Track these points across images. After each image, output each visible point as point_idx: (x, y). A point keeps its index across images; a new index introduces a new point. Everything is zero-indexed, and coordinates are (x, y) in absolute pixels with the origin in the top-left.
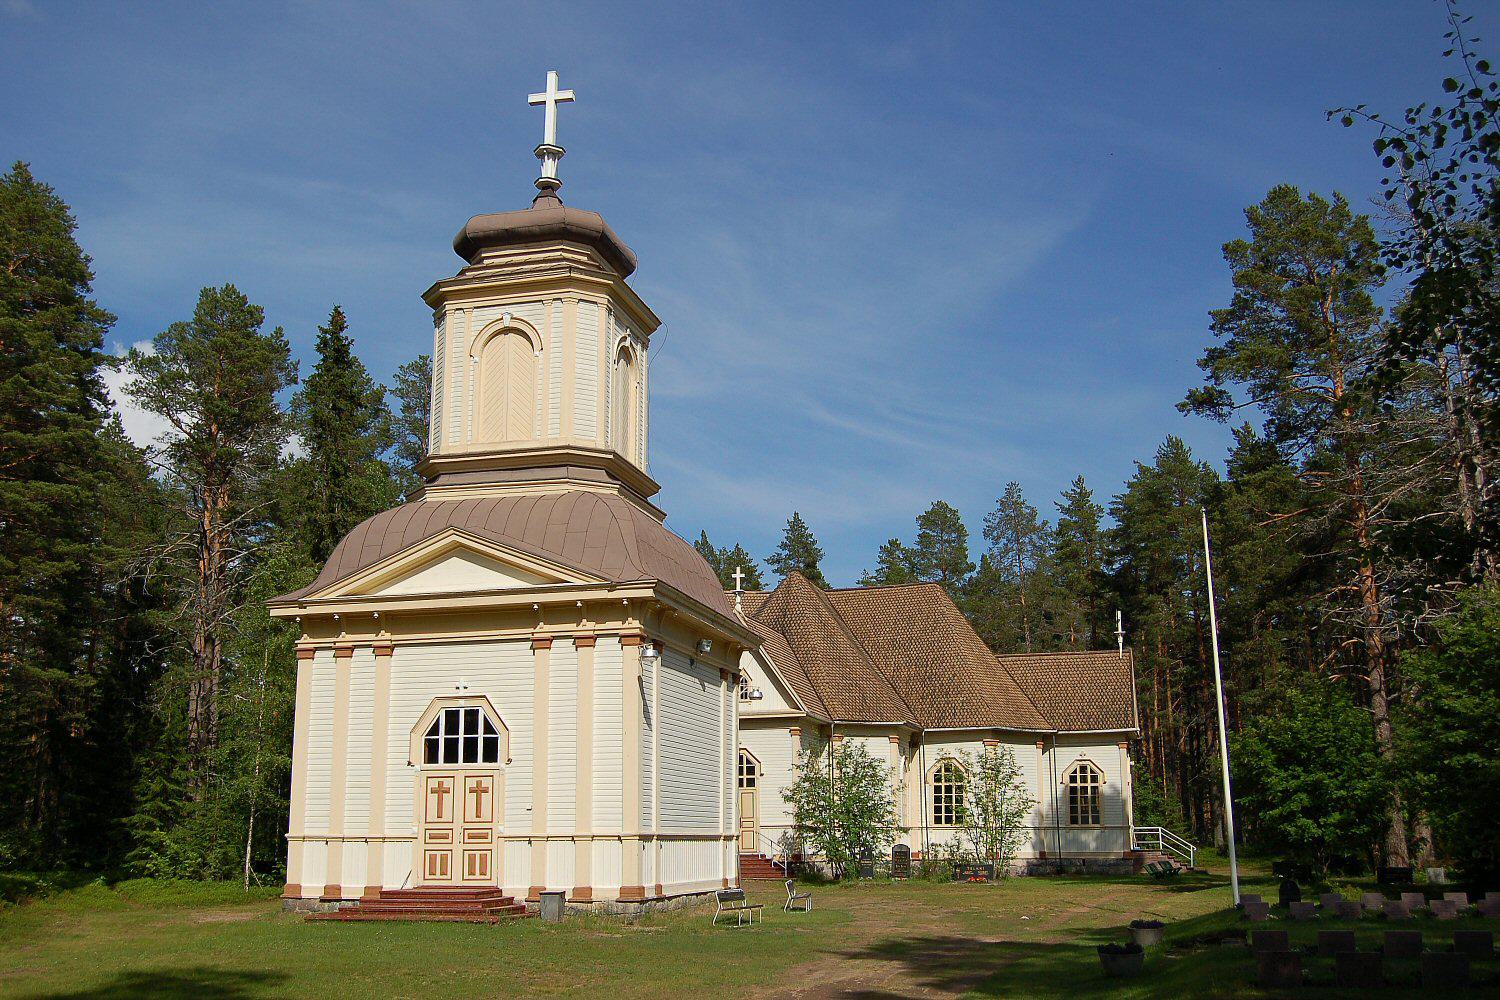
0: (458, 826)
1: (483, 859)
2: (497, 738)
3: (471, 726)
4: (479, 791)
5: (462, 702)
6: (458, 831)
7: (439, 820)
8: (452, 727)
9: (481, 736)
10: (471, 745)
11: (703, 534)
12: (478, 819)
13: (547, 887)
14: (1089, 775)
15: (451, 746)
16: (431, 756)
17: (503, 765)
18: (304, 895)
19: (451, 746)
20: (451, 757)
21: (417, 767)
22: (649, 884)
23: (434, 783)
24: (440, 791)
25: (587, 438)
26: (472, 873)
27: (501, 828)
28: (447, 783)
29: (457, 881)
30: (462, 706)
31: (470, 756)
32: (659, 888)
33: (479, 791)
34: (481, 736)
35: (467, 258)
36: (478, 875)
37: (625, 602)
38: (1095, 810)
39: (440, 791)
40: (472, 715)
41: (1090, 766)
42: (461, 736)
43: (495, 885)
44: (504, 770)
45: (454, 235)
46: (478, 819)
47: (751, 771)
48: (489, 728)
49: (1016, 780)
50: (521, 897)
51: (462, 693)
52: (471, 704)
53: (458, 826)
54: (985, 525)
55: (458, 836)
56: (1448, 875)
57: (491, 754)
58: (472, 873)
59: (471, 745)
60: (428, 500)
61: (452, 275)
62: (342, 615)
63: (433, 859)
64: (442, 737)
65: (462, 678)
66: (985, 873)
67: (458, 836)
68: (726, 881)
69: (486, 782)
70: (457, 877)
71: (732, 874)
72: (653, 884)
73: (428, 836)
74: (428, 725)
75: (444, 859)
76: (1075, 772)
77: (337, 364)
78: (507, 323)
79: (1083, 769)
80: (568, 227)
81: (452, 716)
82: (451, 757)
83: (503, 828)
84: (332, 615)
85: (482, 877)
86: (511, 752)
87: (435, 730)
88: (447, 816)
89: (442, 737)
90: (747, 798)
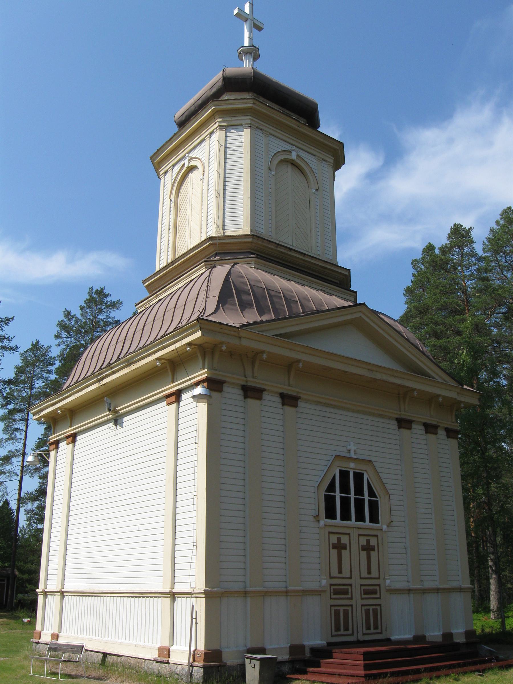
0: (356, 582)
5: (352, 465)
8: (345, 489)
9: (366, 497)
12: (369, 576)
13: (268, 647)
16: (330, 514)
17: (385, 527)
20: (346, 516)
23: (334, 539)
24: (339, 547)
25: (288, 115)
26: (368, 628)
28: (345, 540)
30: (352, 467)
33: (368, 548)
36: (342, 632)
38: (374, 506)
40: (359, 477)
48: (372, 493)
49: (11, 342)
52: (361, 468)
53: (356, 582)
54: (475, 248)
55: (357, 592)
56: (27, 587)
58: (368, 628)
64: (338, 494)
67: (357, 592)
69: (373, 542)
72: (462, 630)
77: (475, 325)
85: (346, 633)
87: (331, 487)
88: (346, 572)
89: (338, 494)
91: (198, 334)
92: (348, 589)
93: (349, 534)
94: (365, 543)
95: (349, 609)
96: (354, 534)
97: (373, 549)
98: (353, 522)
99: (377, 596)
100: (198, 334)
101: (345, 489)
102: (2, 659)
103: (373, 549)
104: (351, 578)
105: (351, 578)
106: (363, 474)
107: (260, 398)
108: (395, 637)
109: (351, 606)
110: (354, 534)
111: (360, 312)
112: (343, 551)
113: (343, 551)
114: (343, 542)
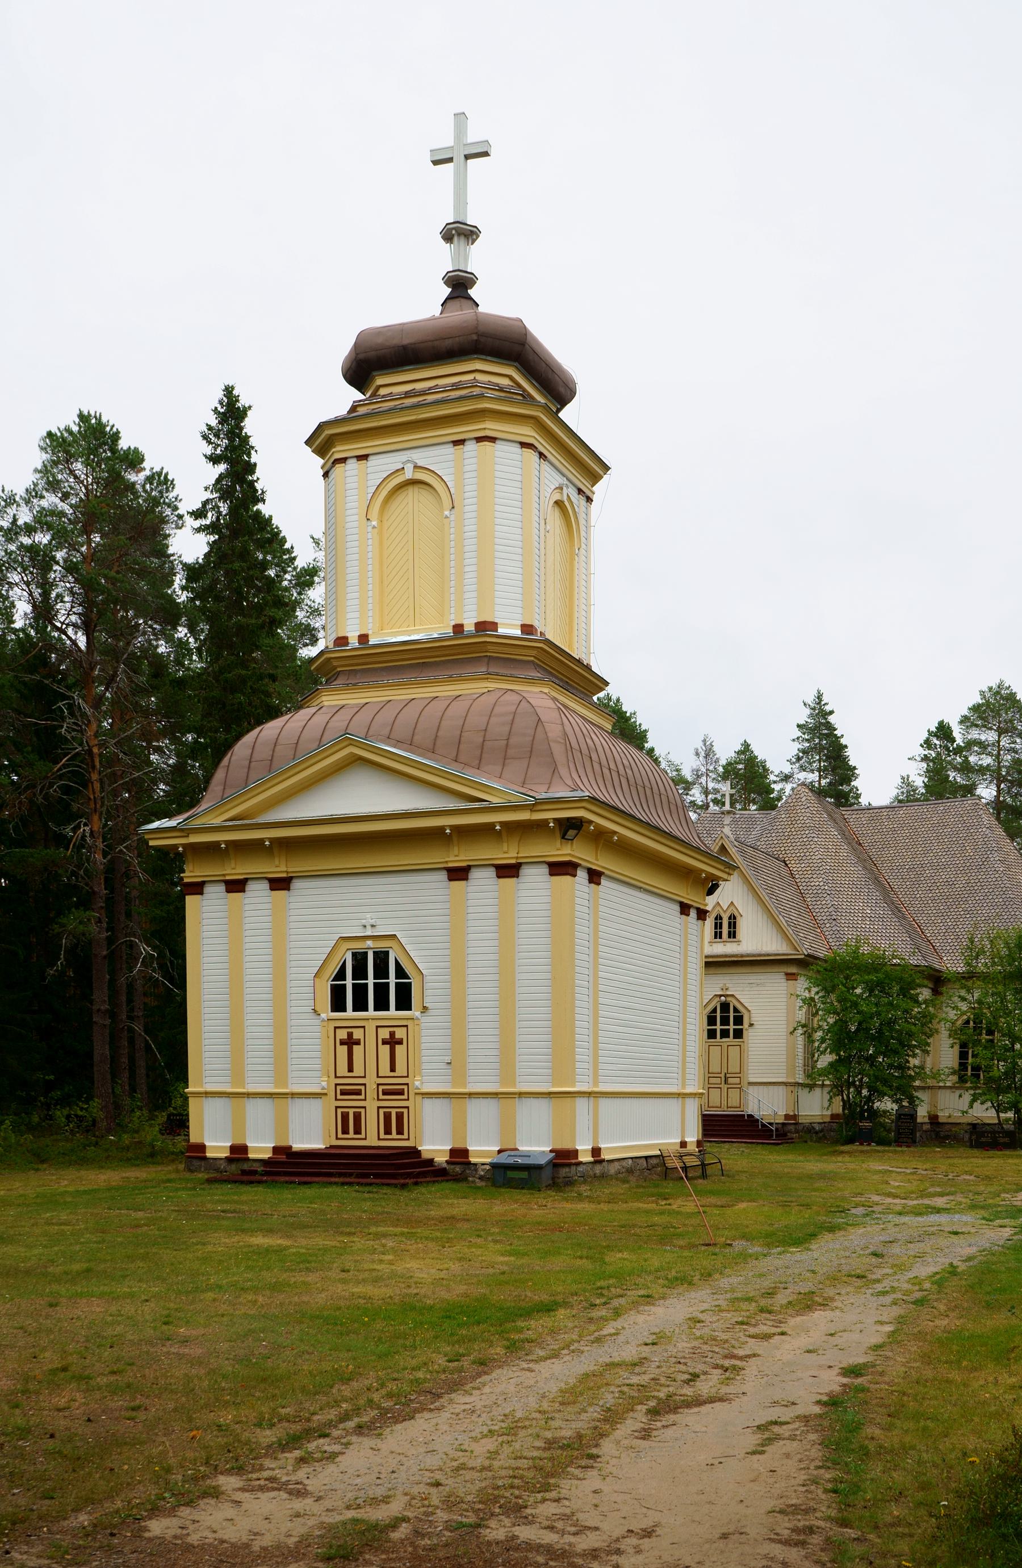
0: (371, 1081)
1: (400, 1117)
2: (410, 983)
3: (381, 970)
4: (393, 1042)
5: (370, 943)
6: (371, 1088)
7: (350, 1074)
8: (360, 971)
9: (392, 980)
10: (381, 991)
11: (842, 735)
12: (392, 1074)
14: (732, 1014)
15: (360, 992)
16: (338, 1004)
17: (417, 1014)
18: (209, 1154)
19: (360, 992)
20: (360, 1005)
21: (323, 1016)
22: (584, 1148)
23: (342, 1034)
24: (350, 1042)
26: (388, 1131)
27: (417, 1083)
28: (357, 1034)
29: (372, 1140)
31: (382, 1004)
32: (596, 1151)
33: (393, 1042)
34: (392, 980)
35: (360, 386)
36: (394, 1135)
37: (498, 827)
39: (350, 1042)
40: (382, 958)
41: (733, 1002)
42: (371, 981)
43: (413, 1145)
44: (418, 1019)
45: (343, 348)
46: (392, 1074)
47: (739, 1020)
48: (400, 972)
50: (441, 1159)
51: (369, 933)
52: (381, 945)
53: (371, 1081)
57: (404, 1002)
58: (388, 1131)
59: (381, 991)
60: (326, 703)
61: (343, 410)
62: (228, 843)
63: (345, 1117)
64: (349, 982)
65: (368, 916)
66: (1006, 1140)
68: (683, 1144)
69: (400, 1033)
70: (372, 1136)
71: (693, 1136)
73: (338, 1092)
74: (333, 969)
75: (357, 1117)
76: (714, 1010)
78: (409, 474)
79: (725, 1007)
80: (482, 339)
81: (360, 960)
82: (360, 1005)
83: (421, 1083)
84: (262, 840)
86: (426, 999)
87: (341, 975)
88: (358, 1070)
89: (349, 982)
90: (734, 1052)
91: (312, 668)
92: (361, 1090)
93: (364, 1027)
94: (397, 1036)
95: (405, 1111)
96: (371, 1027)
97: (400, 1042)
98: (349, 1013)
99: (362, 1097)
100: (312, 668)
101: (360, 971)
102: (2, 1193)
103: (400, 1042)
104: (365, 1077)
105: (365, 1077)
106: (388, 952)
107: (201, 893)
108: (523, 1148)
109: (408, 1107)
110: (371, 1027)
111: (356, 762)
112: (355, 1047)
113: (355, 1047)
114: (355, 1037)
